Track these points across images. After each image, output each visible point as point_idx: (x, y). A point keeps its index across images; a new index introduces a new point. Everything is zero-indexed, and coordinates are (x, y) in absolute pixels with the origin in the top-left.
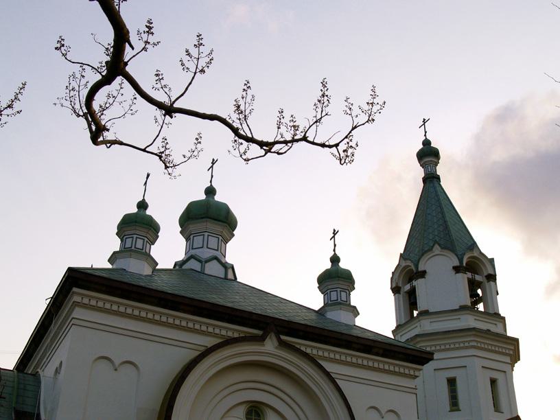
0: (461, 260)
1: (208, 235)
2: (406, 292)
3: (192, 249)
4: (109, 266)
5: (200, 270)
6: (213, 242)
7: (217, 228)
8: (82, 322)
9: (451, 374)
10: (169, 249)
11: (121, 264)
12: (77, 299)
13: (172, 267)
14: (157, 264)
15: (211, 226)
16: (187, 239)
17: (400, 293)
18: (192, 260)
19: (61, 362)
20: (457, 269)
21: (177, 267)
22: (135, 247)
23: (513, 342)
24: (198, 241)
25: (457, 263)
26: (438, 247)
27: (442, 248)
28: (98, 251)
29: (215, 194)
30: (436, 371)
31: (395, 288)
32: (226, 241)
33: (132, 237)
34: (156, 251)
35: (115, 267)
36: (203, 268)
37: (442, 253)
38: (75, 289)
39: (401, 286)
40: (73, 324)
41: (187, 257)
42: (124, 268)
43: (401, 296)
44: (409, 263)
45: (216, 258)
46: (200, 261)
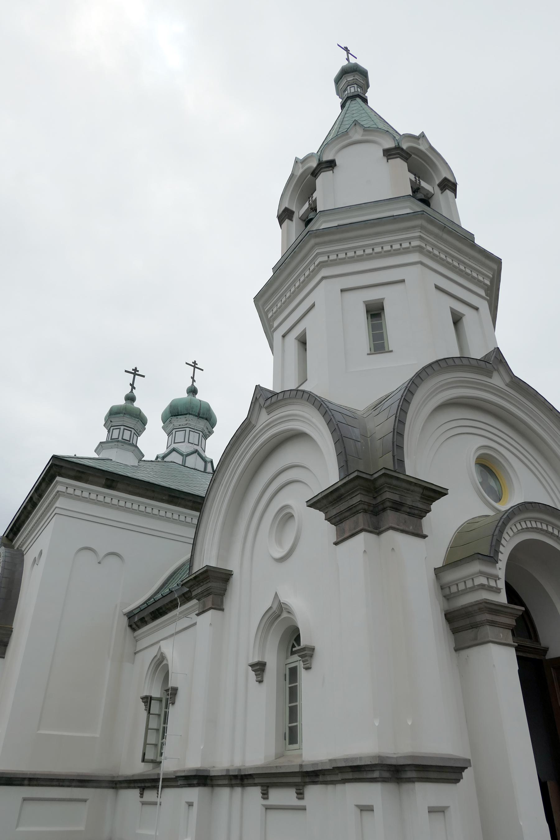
1: (124, 429)
3: (174, 443)
4: (96, 456)
5: (181, 463)
6: (194, 437)
7: (202, 424)
9: (373, 295)
10: (153, 442)
11: (105, 454)
12: (60, 488)
13: (154, 459)
14: (143, 456)
15: (192, 421)
16: (169, 435)
18: (174, 453)
19: (42, 550)
21: (159, 459)
22: (122, 439)
23: (338, 519)
24: (180, 436)
28: (84, 442)
29: (196, 394)
30: (347, 295)
32: (206, 437)
33: (120, 429)
34: (142, 442)
35: (101, 456)
36: (184, 461)
38: (58, 479)
40: (56, 514)
41: (169, 450)
42: (111, 458)
45: (196, 451)
46: (181, 454)
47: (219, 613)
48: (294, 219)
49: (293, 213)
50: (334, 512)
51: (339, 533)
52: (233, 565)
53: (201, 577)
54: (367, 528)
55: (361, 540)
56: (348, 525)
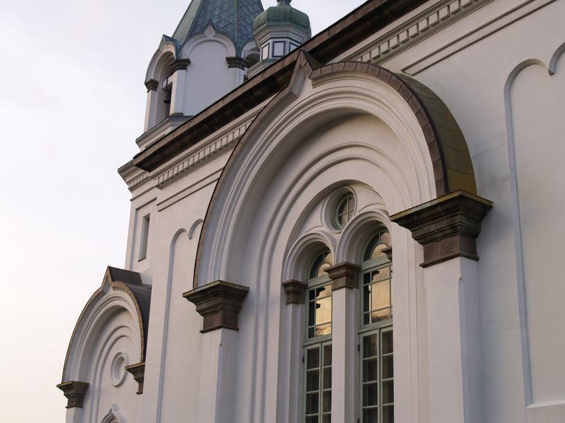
0: (239, 50)
1: (274, 42)
2: (163, 89)
8: (176, 197)
17: (156, 90)
20: (233, 62)
25: (233, 54)
26: (213, 30)
27: (218, 31)
31: (152, 81)
37: (217, 39)
39: (158, 80)
43: (157, 94)
44: (172, 49)
47: (233, 332)
48: (158, 90)
49: (157, 83)
50: (204, 306)
51: (427, 254)
52: (251, 284)
53: (426, 215)
54: (462, 252)
55: (454, 267)
56: (439, 247)
